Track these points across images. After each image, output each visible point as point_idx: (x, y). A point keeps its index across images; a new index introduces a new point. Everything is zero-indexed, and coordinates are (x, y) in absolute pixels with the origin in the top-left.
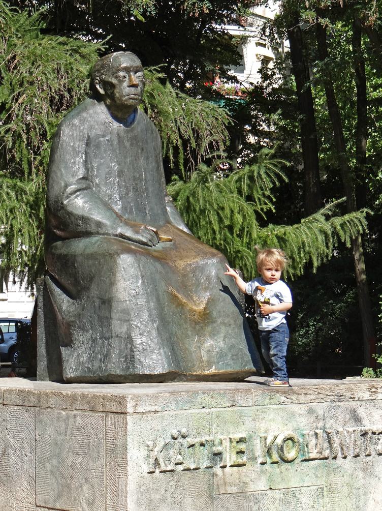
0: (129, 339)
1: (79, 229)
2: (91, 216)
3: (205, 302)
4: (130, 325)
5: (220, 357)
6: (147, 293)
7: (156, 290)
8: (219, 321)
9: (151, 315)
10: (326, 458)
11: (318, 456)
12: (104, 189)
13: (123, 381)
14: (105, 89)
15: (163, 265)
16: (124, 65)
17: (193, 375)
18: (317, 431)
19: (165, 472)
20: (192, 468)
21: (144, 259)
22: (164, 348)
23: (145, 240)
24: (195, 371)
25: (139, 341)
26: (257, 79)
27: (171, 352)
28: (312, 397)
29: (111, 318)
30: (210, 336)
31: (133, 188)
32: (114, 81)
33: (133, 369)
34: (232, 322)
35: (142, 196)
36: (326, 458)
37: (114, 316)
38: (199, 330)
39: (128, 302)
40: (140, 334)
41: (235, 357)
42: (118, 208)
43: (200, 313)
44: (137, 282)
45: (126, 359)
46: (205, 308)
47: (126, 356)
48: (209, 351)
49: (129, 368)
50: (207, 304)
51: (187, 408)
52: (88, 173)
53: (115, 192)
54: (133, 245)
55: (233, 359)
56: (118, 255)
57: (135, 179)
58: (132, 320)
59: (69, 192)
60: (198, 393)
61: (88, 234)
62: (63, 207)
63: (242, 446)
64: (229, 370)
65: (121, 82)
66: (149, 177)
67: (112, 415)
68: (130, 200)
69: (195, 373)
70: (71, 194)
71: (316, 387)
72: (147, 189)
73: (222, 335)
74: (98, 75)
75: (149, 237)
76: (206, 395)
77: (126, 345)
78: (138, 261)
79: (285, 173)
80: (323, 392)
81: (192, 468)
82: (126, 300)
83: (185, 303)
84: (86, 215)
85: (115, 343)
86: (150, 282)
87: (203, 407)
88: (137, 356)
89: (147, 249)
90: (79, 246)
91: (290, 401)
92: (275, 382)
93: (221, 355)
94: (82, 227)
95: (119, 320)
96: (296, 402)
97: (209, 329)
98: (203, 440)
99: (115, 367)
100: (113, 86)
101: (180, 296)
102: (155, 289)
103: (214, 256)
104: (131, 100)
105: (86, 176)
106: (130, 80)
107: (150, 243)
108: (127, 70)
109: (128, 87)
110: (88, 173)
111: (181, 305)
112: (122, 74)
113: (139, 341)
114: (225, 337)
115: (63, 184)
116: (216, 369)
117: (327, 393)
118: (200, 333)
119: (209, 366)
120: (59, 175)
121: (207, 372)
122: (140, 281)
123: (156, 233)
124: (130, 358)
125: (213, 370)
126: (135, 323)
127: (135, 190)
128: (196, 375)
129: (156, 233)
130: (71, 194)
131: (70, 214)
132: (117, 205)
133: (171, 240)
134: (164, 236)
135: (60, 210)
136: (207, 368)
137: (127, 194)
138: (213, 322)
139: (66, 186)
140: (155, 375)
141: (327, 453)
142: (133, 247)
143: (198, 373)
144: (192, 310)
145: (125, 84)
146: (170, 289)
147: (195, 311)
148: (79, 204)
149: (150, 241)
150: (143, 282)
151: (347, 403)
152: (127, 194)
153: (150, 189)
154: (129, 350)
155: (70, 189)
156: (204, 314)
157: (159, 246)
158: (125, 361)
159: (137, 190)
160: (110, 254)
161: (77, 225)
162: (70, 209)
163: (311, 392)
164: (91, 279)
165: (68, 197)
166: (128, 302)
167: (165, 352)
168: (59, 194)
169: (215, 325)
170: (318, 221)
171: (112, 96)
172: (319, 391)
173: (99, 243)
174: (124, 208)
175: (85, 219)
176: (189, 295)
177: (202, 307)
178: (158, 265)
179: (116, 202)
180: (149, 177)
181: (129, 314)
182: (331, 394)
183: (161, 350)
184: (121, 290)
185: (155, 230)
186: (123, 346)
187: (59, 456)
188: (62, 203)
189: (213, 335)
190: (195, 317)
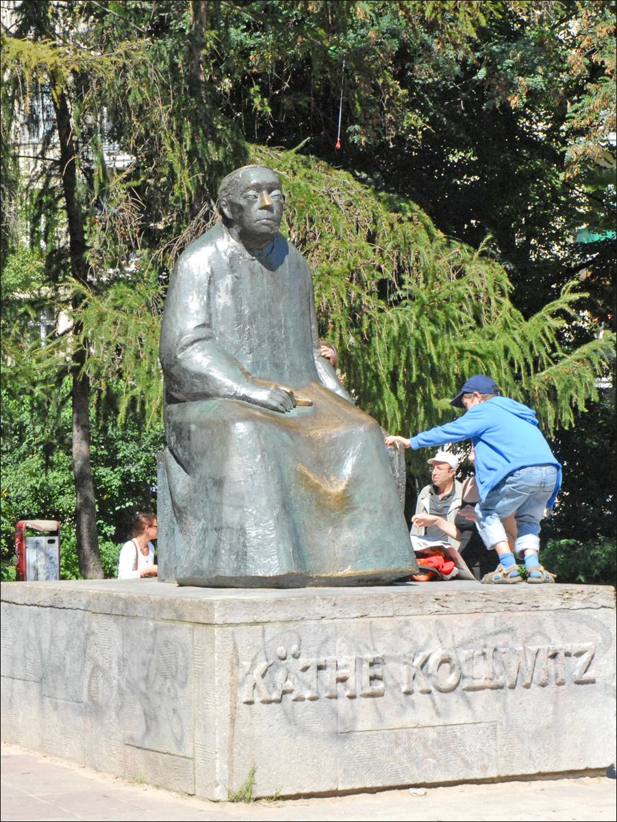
0: (242, 531)
1: (195, 390)
2: (211, 374)
3: (345, 483)
5: (360, 554)
6: (267, 472)
7: (280, 468)
8: (362, 506)
9: (270, 500)
10: (501, 687)
11: (488, 683)
12: (231, 339)
13: (233, 585)
14: (232, 212)
15: (291, 437)
16: (254, 182)
17: (322, 578)
18: (485, 650)
19: (269, 702)
20: (306, 697)
21: (266, 428)
22: (284, 542)
25: (253, 534)
27: (293, 548)
28: (478, 605)
29: (222, 504)
30: (349, 526)
31: (269, 338)
32: (243, 202)
33: (245, 569)
34: (379, 508)
35: (279, 348)
36: (501, 687)
37: (226, 501)
38: (334, 519)
39: (242, 483)
40: (255, 524)
41: (379, 554)
42: (247, 362)
43: (337, 496)
44: (255, 457)
45: (237, 556)
46: (345, 491)
47: (238, 552)
48: (346, 546)
49: (240, 568)
50: (347, 485)
52: (210, 318)
53: (244, 343)
54: (258, 410)
55: (376, 556)
56: (233, 421)
57: (272, 326)
58: (246, 507)
59: (184, 343)
60: (315, 598)
61: (206, 396)
62: (177, 362)
63: (377, 671)
65: (251, 203)
66: (290, 323)
67: (200, 627)
68: (263, 353)
69: (324, 575)
70: (187, 345)
71: (483, 592)
72: (287, 339)
73: (364, 525)
74: (225, 194)
75: (281, 400)
76: (325, 602)
77: (239, 539)
78: (259, 430)
80: (494, 599)
81: (306, 697)
83: (317, 484)
84: (204, 372)
85: (225, 536)
86: (274, 459)
87: (323, 618)
88: (251, 553)
89: (277, 416)
90: (195, 412)
91: (446, 609)
92: (167, 598)
93: (361, 551)
94: (199, 387)
95: (231, 506)
96: (455, 611)
97: (347, 518)
98: (321, 660)
99: (226, 568)
100: (241, 208)
101: (311, 476)
102: (279, 466)
103: (361, 422)
104: (263, 226)
105: (207, 322)
106: (263, 201)
107: (281, 408)
108: (258, 188)
109: (260, 209)
110: (210, 318)
111: (315, 488)
112: (251, 193)
113: (253, 534)
114: (368, 527)
115: (178, 333)
116: (352, 569)
118: (335, 523)
119: (344, 566)
120: (173, 321)
121: (340, 574)
122: (259, 456)
123: (291, 395)
124: (241, 556)
125: (348, 571)
126: (250, 510)
127: (272, 339)
128: (325, 578)
129: (291, 395)
130: (187, 345)
131: (185, 371)
132: (247, 359)
133: (311, 404)
134: (301, 398)
135: (174, 365)
136: (341, 568)
137: (260, 345)
138: (352, 509)
139: (181, 335)
140: (270, 577)
142: (258, 413)
143: (329, 575)
144: (327, 494)
145: (256, 206)
146: (300, 467)
147: (330, 494)
148: (198, 360)
149: (281, 405)
150: (263, 457)
151: (528, 613)
152: (260, 345)
153: (292, 340)
154: (241, 544)
155: (185, 340)
156: (343, 499)
157: (294, 413)
158: (236, 559)
159: (273, 340)
160: (224, 422)
161: (193, 384)
162: (185, 364)
163: (476, 598)
164: (203, 454)
165: (183, 349)
166: (242, 483)
167: (285, 548)
168: (173, 345)
169: (356, 512)
171: (240, 222)
172: (488, 597)
173: (216, 407)
174: (255, 364)
175: (202, 377)
176: (325, 474)
177: (341, 488)
178: (285, 435)
179: (245, 355)
180: (290, 323)
181: (243, 499)
182: (505, 600)
183: (280, 545)
185: (288, 391)
186: (235, 540)
187: (146, 679)
188: (176, 357)
189: (352, 524)
190: (331, 502)
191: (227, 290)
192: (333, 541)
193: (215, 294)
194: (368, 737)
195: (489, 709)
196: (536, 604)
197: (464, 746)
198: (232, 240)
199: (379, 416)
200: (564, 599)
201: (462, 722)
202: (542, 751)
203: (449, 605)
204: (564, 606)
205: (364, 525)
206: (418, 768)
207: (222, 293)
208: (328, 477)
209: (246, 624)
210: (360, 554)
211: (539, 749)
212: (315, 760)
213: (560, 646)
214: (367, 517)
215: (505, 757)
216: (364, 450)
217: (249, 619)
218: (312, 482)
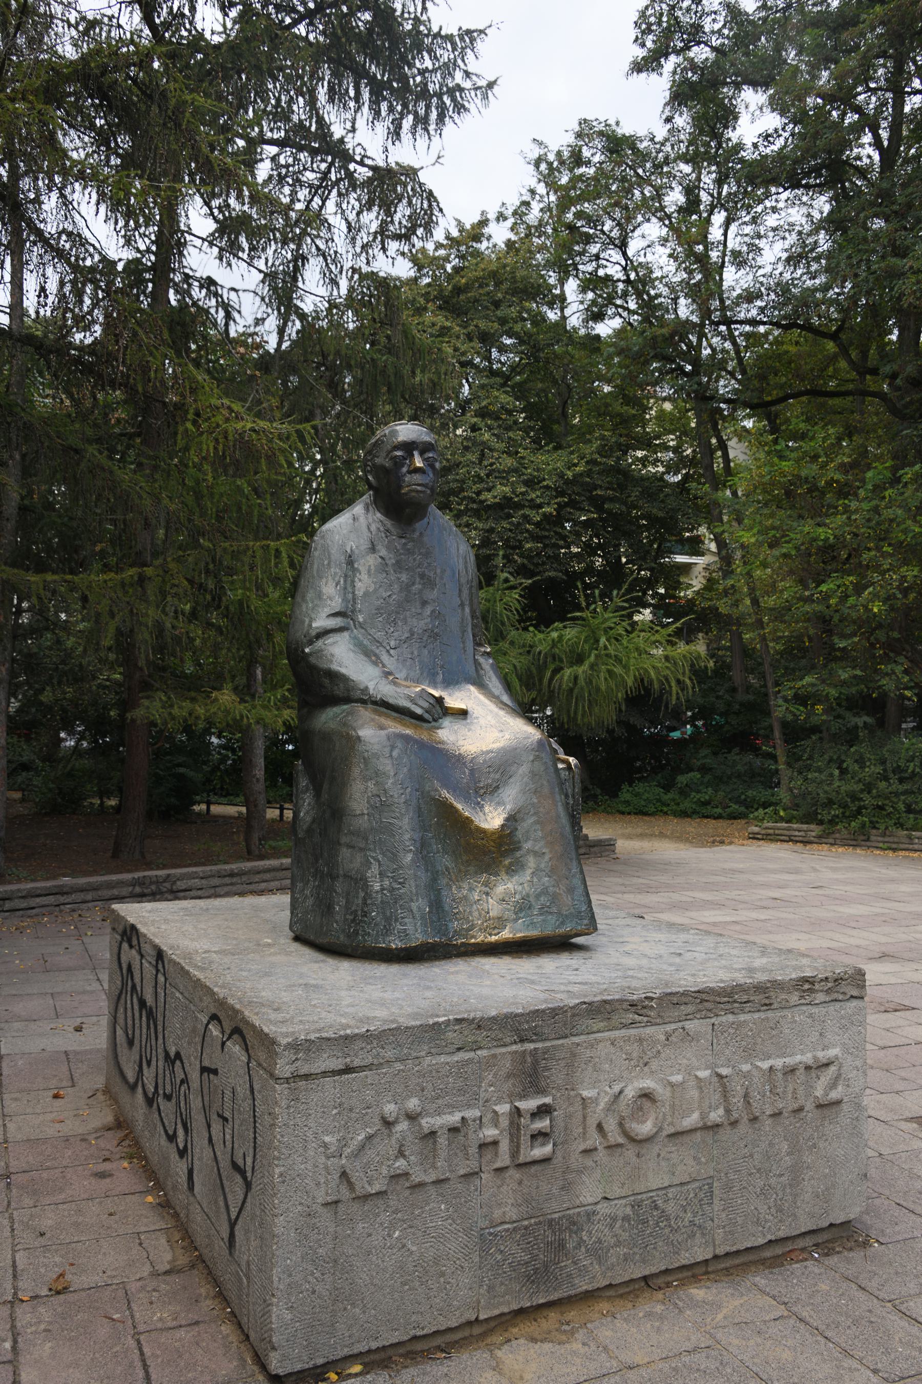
4: (366, 856)
8: (527, 846)
23: (419, 711)
24: (473, 937)
25: (377, 886)
26: (323, 291)
51: (423, 1054)
58: (369, 850)
64: (534, 933)
69: (473, 941)
73: (529, 872)
79: (446, 755)
82: (363, 814)
83: (467, 818)
90: (328, 718)
91: (645, 1019)
93: (523, 907)
101: (459, 806)
107: (427, 716)
117: (718, 999)
119: (500, 922)
125: (506, 934)
136: (496, 931)
141: (717, 1115)
169: (518, 854)
170: (669, 863)
172: (704, 996)
181: (366, 839)
182: (726, 999)
184: (357, 795)
189: (511, 871)
191: (369, 571)
192: (487, 894)
193: (354, 576)
194: (526, 1228)
195: (703, 1160)
196: (767, 1002)
197: (668, 1220)
198: (379, 515)
199: (838, 1253)
200: (804, 991)
201: (666, 1185)
202: (773, 1210)
203: (649, 1013)
204: (803, 1001)
205: (529, 872)
206: (600, 1264)
207: (364, 576)
208: (482, 807)
209: (335, 1073)
210: (521, 910)
211: (769, 1208)
212: (442, 1280)
213: (798, 1058)
214: (531, 862)
215: (724, 1227)
216: (533, 774)
217: (337, 1064)
218: (461, 815)
